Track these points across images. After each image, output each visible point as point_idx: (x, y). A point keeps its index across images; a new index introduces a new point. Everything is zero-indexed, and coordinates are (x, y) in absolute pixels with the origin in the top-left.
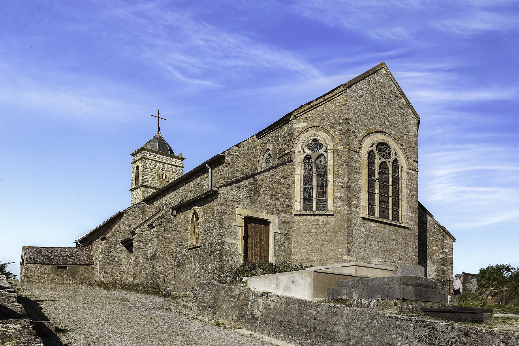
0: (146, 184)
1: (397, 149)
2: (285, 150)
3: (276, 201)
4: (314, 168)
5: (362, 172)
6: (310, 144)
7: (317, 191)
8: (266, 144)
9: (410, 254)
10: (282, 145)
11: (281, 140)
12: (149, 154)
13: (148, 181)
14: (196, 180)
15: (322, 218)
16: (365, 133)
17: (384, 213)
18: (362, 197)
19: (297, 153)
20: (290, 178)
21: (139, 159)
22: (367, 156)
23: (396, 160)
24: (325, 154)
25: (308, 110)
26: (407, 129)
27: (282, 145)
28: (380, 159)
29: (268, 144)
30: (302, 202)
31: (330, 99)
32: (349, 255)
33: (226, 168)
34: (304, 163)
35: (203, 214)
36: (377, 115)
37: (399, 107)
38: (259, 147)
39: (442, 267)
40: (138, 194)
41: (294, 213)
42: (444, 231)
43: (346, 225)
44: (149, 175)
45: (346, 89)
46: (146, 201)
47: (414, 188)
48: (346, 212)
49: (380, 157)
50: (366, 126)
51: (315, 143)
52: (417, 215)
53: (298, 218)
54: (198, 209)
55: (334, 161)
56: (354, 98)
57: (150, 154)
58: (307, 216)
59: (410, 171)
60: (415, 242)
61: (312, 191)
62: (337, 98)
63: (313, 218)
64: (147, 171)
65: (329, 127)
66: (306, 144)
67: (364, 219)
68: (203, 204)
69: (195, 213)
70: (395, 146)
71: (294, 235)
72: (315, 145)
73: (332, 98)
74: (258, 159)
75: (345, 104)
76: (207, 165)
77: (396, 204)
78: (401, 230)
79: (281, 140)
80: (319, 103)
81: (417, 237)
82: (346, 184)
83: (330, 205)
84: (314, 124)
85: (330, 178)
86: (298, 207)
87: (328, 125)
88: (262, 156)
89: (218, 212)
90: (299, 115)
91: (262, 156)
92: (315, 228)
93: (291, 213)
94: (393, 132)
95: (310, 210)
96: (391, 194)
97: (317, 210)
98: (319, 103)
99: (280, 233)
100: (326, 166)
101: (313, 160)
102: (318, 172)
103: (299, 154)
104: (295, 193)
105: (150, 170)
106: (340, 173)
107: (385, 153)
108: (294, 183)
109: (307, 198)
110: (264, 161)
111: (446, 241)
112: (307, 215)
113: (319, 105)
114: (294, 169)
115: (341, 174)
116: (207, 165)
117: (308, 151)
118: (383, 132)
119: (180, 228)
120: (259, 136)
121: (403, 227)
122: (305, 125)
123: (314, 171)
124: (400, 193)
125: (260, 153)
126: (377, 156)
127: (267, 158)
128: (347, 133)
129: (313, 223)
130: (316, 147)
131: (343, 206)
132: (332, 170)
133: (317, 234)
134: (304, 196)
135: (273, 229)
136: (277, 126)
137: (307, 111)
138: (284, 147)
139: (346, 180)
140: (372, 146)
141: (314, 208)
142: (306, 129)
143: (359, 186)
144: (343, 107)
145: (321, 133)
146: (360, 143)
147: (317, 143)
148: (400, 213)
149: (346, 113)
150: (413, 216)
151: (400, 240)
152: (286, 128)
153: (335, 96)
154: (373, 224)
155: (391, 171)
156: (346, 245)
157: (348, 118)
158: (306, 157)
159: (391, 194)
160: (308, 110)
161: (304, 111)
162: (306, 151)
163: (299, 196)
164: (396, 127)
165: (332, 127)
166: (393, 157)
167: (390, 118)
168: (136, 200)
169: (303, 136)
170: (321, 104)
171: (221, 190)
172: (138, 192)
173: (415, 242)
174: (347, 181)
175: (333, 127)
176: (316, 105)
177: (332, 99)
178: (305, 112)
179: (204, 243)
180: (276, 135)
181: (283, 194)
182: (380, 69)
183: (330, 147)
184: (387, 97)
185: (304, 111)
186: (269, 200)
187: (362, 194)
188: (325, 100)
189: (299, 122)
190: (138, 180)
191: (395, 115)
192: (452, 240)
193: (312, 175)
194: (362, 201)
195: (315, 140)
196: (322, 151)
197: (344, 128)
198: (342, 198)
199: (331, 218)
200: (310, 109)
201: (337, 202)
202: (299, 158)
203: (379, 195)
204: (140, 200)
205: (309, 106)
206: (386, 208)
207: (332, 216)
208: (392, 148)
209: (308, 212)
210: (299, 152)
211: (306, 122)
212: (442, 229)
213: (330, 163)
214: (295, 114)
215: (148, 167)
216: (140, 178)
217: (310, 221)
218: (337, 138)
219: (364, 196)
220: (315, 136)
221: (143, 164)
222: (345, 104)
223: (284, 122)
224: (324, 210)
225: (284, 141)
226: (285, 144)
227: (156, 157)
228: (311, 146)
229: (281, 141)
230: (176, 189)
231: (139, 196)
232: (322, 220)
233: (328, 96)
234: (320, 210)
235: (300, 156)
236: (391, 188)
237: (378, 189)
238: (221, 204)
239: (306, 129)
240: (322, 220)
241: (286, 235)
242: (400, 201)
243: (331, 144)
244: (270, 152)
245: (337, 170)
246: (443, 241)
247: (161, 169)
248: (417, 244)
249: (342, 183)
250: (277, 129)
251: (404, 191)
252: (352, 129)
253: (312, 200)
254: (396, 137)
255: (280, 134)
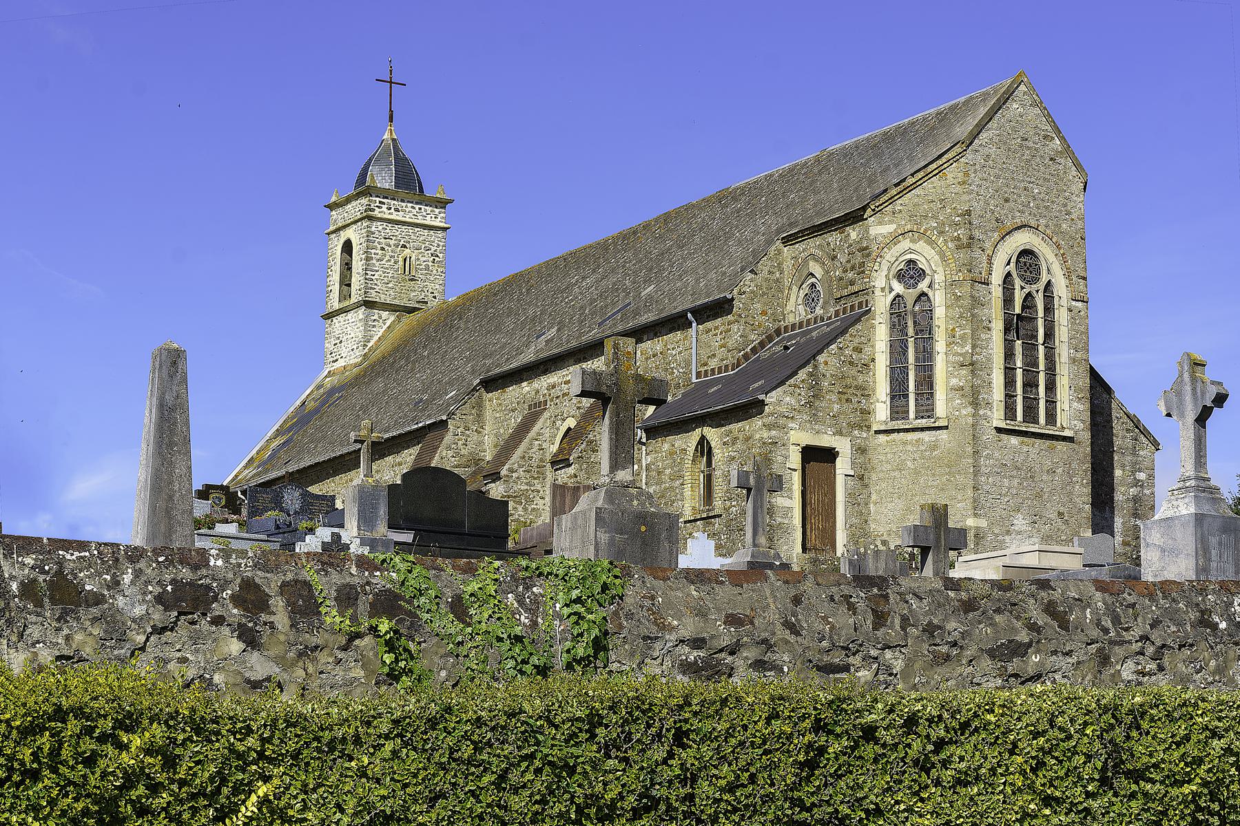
0: (373, 296)
1: (1051, 257)
2: (852, 283)
3: (846, 405)
4: (910, 324)
5: (993, 325)
6: (902, 270)
7: (916, 376)
8: (805, 261)
9: (1078, 500)
10: (845, 271)
11: (842, 258)
12: (377, 204)
13: (375, 287)
14: (649, 342)
15: (926, 436)
16: (996, 235)
17: (1031, 413)
18: (994, 382)
19: (878, 292)
20: (867, 349)
21: (355, 222)
22: (1001, 289)
23: (1049, 283)
24: (930, 294)
25: (898, 196)
26: (1065, 205)
27: (845, 271)
28: (1022, 288)
29: (811, 263)
30: (888, 403)
31: (937, 171)
32: (975, 515)
33: (735, 327)
34: (891, 314)
35: (724, 444)
36: (1015, 191)
37: (1051, 159)
38: (788, 265)
39: (1133, 520)
40: (349, 328)
41: (875, 428)
42: (1137, 427)
43: (969, 449)
44: (377, 269)
45: (965, 150)
46: (484, 382)
47: (1081, 343)
48: (970, 420)
49: (1023, 284)
50: (997, 220)
51: (910, 268)
52: (1088, 405)
53: (882, 438)
54: (713, 435)
55: (947, 307)
56: (977, 167)
57: (380, 202)
58: (898, 432)
59: (1074, 303)
60: (1085, 471)
61: (908, 376)
62: (948, 169)
63: (910, 436)
64: (373, 256)
65: (936, 233)
66: (894, 271)
67: (999, 430)
68: (723, 422)
69: (703, 443)
70: (1047, 253)
71: (874, 477)
72: (911, 273)
73: (940, 169)
74: (785, 294)
75: (964, 183)
76: (689, 315)
77: (1051, 387)
78: (1060, 445)
79: (842, 258)
80: (917, 181)
81: (1089, 458)
82: (968, 357)
83: (941, 408)
84: (909, 227)
85: (940, 346)
86: (882, 412)
87: (935, 228)
88: (795, 288)
89: (764, 443)
90: (880, 208)
91: (795, 288)
92: (914, 460)
93: (869, 427)
94: (1043, 221)
95: (903, 418)
96: (1042, 367)
97: (916, 418)
98: (917, 181)
99: (853, 476)
100: (932, 319)
101: (909, 307)
102: (917, 334)
103: (882, 294)
104: (875, 382)
105: (380, 252)
106: (958, 333)
107: (1031, 272)
108: (873, 360)
109: (898, 393)
110: (800, 301)
111: (1141, 453)
112: (899, 431)
113: (918, 184)
114: (873, 327)
115: (960, 335)
116: (689, 315)
117: (898, 288)
118: (1025, 226)
119: (659, 473)
120: (788, 241)
121: (1065, 439)
122: (891, 228)
123: (911, 331)
124: (1057, 359)
125: (790, 280)
126: (1018, 283)
127: (807, 294)
128: (969, 246)
129: (909, 448)
130: (912, 278)
131: (964, 408)
132: (943, 327)
133: (917, 472)
134: (891, 387)
135: (843, 466)
136: (834, 225)
137: (896, 198)
138: (850, 275)
139: (968, 348)
140: (1008, 264)
141: (912, 415)
142: (895, 239)
143: (989, 359)
144: (959, 189)
145: (921, 246)
146: (990, 259)
147: (914, 268)
148: (1058, 404)
149: (965, 202)
150: (1081, 407)
151: (1060, 471)
152: (853, 233)
153: (945, 166)
154: (1014, 440)
155: (1041, 313)
156: (970, 493)
157: (969, 213)
158: (894, 300)
159: (1042, 367)
160: (898, 196)
161: (890, 199)
162: (893, 288)
163: (882, 388)
164: (1046, 207)
165: (941, 233)
166: (1044, 278)
167: (1037, 191)
168: (344, 348)
169: (890, 255)
170: (919, 183)
171: (769, 398)
172: (350, 321)
173: (1085, 471)
174: (970, 351)
175: (942, 232)
176: (911, 185)
177: (940, 172)
178: (892, 200)
179: (730, 508)
180: (828, 244)
181: (856, 386)
182: (1018, 87)
183: (939, 278)
184: (1030, 144)
185: (890, 199)
186: (836, 406)
187: (994, 374)
188: (927, 175)
189: (880, 223)
190: (349, 285)
191: (1045, 179)
192: (1153, 448)
193: (907, 341)
194: (994, 391)
195: (911, 262)
196: (923, 286)
197: (963, 234)
198: (962, 388)
199: (943, 435)
200: (901, 195)
201: (952, 399)
202: (881, 304)
203: (1023, 370)
204: (355, 347)
205: (899, 189)
206: (1035, 399)
207: (945, 431)
208: (1042, 259)
209: (899, 424)
210: (883, 289)
211: (891, 222)
212: (1133, 422)
213: (940, 312)
214: (873, 207)
215: (376, 244)
216: (356, 281)
217: (905, 443)
218: (951, 257)
219: (998, 378)
220: (911, 253)
221: (367, 236)
222: (964, 183)
223: (850, 219)
224: (929, 417)
225: (848, 261)
226: (853, 268)
227: (392, 210)
228: (903, 276)
229: (843, 260)
230: (585, 358)
231: (353, 335)
232: (927, 439)
233: (934, 166)
234: (922, 417)
235: (883, 299)
236: (1041, 349)
237: (1021, 356)
238: (769, 427)
239: (895, 239)
240: (927, 439)
241: (861, 478)
242: (1058, 378)
243: (940, 270)
244: (813, 280)
245: (951, 327)
246: (1134, 453)
247: (402, 243)
248: (1089, 473)
249: (961, 355)
250: (832, 231)
251: (1064, 353)
252: (977, 234)
253: (907, 396)
254: (1048, 231)
255: (838, 243)
